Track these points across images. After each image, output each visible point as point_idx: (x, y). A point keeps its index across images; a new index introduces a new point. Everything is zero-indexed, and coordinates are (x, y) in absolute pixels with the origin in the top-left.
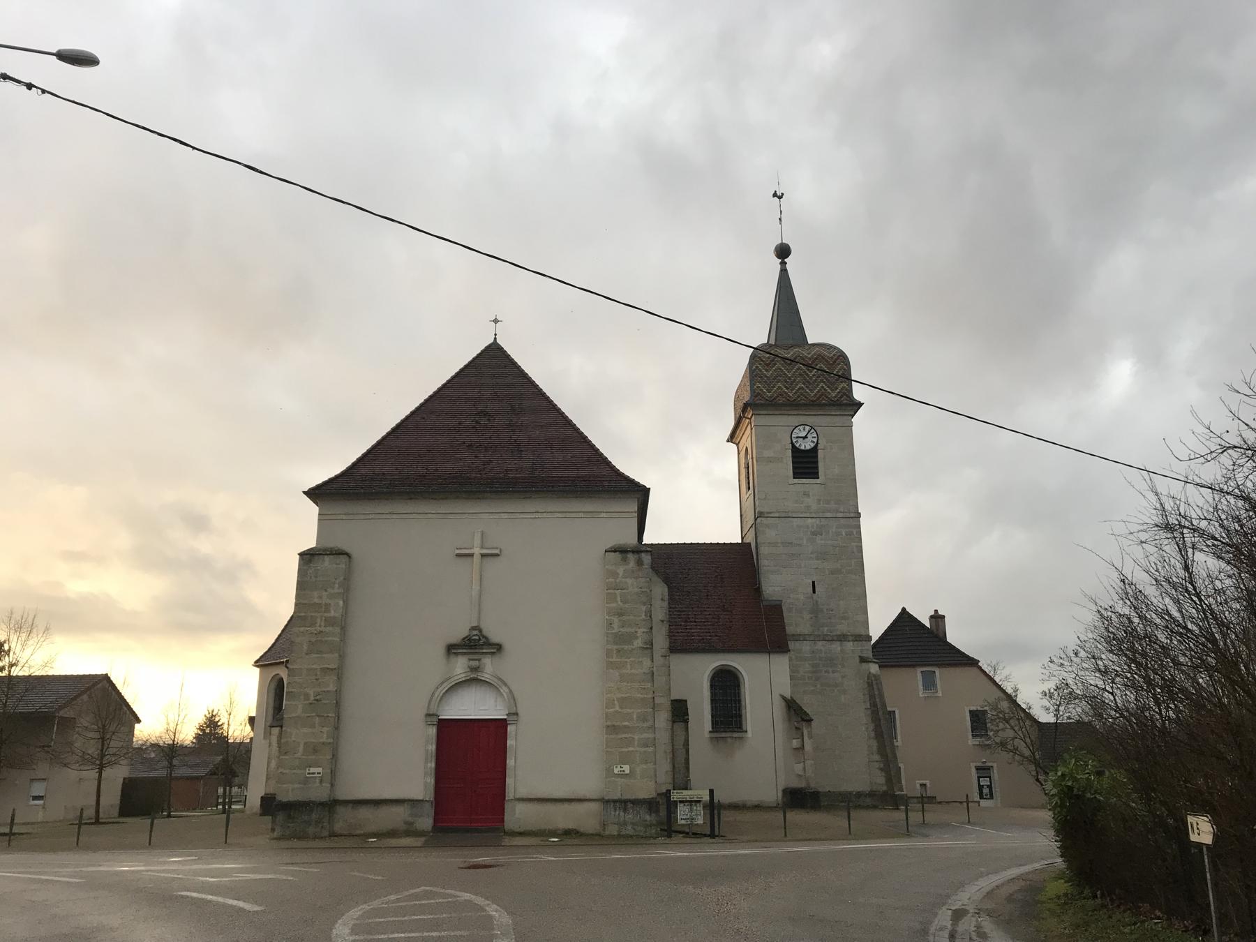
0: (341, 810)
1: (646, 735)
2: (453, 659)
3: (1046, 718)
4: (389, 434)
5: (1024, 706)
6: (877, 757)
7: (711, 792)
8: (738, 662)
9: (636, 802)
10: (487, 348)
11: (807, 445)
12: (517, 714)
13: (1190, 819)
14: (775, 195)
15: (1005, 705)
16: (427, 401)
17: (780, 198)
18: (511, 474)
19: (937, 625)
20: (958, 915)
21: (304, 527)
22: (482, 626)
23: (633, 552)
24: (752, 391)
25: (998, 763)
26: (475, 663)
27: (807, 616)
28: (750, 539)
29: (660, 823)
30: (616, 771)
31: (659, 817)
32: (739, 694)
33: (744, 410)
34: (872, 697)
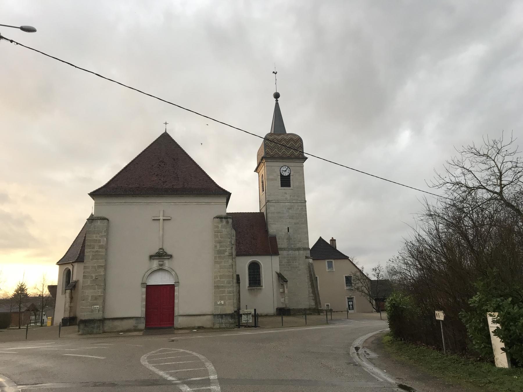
0: (107, 322)
1: (230, 289)
2: (152, 261)
4: (123, 170)
5: (365, 274)
6: (312, 295)
7: (255, 310)
8: (259, 259)
9: (226, 315)
10: (163, 134)
11: (286, 174)
12: (178, 282)
13: (436, 312)
14: (274, 72)
15: (359, 274)
16: (138, 156)
17: (276, 73)
18: (175, 187)
19: (333, 243)
20: (357, 349)
21: (88, 207)
22: (164, 248)
24: (265, 152)
25: (356, 296)
26: (161, 263)
27: (285, 241)
28: (263, 210)
30: (218, 303)
31: (235, 320)
33: (262, 160)
34: (310, 271)
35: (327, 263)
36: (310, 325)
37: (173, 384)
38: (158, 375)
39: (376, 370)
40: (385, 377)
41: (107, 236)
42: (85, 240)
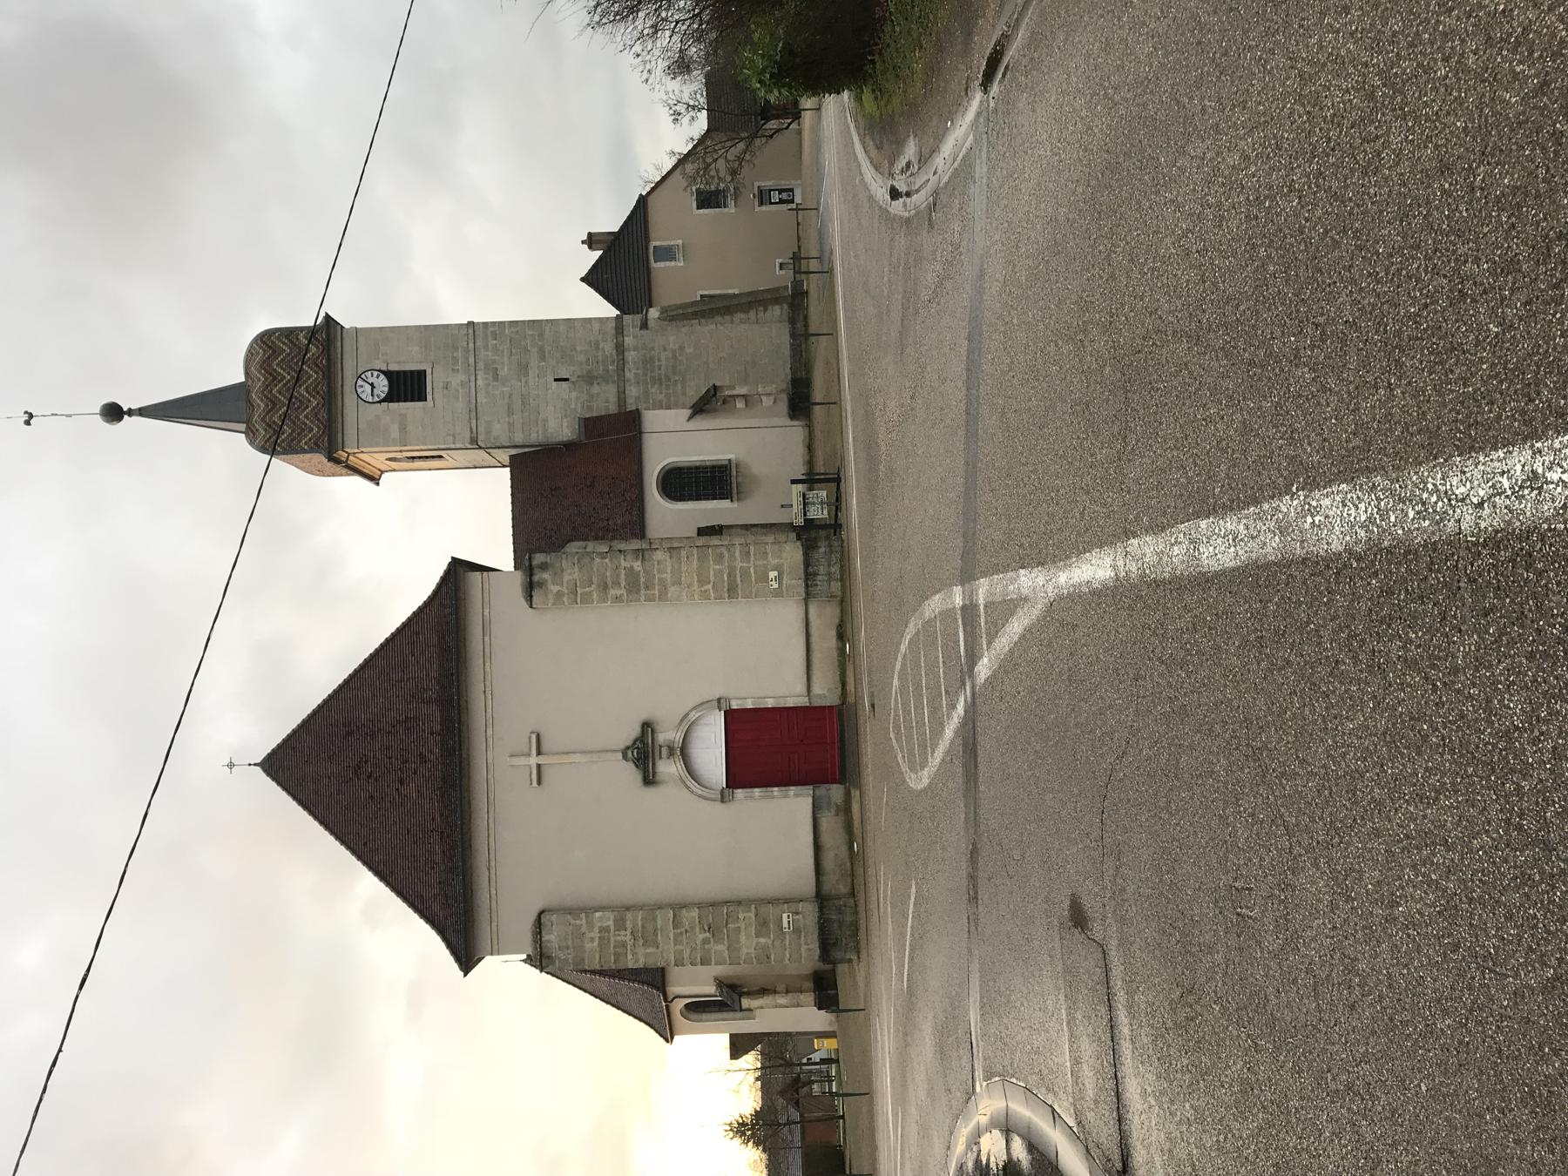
0: (826, 888)
3: (702, 123)
5: (690, 146)
6: (752, 314)
7: (794, 482)
9: (807, 563)
10: (268, 774)
11: (383, 385)
12: (719, 700)
14: (28, 423)
15: (690, 168)
16: (343, 842)
17: (31, 416)
19: (600, 242)
20: (895, 194)
21: (505, 971)
23: (531, 575)
24: (311, 451)
25: (755, 180)
26: (665, 751)
27: (595, 389)
28: (504, 456)
29: (828, 538)
31: (820, 537)
32: (689, 468)
33: (337, 461)
34: (685, 317)
35: (661, 265)
36: (835, 322)
37: (974, 702)
38: (952, 743)
39: (947, 148)
40: (965, 126)
41: (587, 910)
42: (602, 973)
